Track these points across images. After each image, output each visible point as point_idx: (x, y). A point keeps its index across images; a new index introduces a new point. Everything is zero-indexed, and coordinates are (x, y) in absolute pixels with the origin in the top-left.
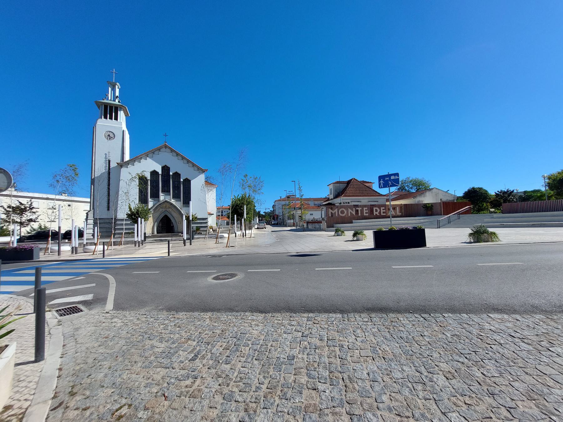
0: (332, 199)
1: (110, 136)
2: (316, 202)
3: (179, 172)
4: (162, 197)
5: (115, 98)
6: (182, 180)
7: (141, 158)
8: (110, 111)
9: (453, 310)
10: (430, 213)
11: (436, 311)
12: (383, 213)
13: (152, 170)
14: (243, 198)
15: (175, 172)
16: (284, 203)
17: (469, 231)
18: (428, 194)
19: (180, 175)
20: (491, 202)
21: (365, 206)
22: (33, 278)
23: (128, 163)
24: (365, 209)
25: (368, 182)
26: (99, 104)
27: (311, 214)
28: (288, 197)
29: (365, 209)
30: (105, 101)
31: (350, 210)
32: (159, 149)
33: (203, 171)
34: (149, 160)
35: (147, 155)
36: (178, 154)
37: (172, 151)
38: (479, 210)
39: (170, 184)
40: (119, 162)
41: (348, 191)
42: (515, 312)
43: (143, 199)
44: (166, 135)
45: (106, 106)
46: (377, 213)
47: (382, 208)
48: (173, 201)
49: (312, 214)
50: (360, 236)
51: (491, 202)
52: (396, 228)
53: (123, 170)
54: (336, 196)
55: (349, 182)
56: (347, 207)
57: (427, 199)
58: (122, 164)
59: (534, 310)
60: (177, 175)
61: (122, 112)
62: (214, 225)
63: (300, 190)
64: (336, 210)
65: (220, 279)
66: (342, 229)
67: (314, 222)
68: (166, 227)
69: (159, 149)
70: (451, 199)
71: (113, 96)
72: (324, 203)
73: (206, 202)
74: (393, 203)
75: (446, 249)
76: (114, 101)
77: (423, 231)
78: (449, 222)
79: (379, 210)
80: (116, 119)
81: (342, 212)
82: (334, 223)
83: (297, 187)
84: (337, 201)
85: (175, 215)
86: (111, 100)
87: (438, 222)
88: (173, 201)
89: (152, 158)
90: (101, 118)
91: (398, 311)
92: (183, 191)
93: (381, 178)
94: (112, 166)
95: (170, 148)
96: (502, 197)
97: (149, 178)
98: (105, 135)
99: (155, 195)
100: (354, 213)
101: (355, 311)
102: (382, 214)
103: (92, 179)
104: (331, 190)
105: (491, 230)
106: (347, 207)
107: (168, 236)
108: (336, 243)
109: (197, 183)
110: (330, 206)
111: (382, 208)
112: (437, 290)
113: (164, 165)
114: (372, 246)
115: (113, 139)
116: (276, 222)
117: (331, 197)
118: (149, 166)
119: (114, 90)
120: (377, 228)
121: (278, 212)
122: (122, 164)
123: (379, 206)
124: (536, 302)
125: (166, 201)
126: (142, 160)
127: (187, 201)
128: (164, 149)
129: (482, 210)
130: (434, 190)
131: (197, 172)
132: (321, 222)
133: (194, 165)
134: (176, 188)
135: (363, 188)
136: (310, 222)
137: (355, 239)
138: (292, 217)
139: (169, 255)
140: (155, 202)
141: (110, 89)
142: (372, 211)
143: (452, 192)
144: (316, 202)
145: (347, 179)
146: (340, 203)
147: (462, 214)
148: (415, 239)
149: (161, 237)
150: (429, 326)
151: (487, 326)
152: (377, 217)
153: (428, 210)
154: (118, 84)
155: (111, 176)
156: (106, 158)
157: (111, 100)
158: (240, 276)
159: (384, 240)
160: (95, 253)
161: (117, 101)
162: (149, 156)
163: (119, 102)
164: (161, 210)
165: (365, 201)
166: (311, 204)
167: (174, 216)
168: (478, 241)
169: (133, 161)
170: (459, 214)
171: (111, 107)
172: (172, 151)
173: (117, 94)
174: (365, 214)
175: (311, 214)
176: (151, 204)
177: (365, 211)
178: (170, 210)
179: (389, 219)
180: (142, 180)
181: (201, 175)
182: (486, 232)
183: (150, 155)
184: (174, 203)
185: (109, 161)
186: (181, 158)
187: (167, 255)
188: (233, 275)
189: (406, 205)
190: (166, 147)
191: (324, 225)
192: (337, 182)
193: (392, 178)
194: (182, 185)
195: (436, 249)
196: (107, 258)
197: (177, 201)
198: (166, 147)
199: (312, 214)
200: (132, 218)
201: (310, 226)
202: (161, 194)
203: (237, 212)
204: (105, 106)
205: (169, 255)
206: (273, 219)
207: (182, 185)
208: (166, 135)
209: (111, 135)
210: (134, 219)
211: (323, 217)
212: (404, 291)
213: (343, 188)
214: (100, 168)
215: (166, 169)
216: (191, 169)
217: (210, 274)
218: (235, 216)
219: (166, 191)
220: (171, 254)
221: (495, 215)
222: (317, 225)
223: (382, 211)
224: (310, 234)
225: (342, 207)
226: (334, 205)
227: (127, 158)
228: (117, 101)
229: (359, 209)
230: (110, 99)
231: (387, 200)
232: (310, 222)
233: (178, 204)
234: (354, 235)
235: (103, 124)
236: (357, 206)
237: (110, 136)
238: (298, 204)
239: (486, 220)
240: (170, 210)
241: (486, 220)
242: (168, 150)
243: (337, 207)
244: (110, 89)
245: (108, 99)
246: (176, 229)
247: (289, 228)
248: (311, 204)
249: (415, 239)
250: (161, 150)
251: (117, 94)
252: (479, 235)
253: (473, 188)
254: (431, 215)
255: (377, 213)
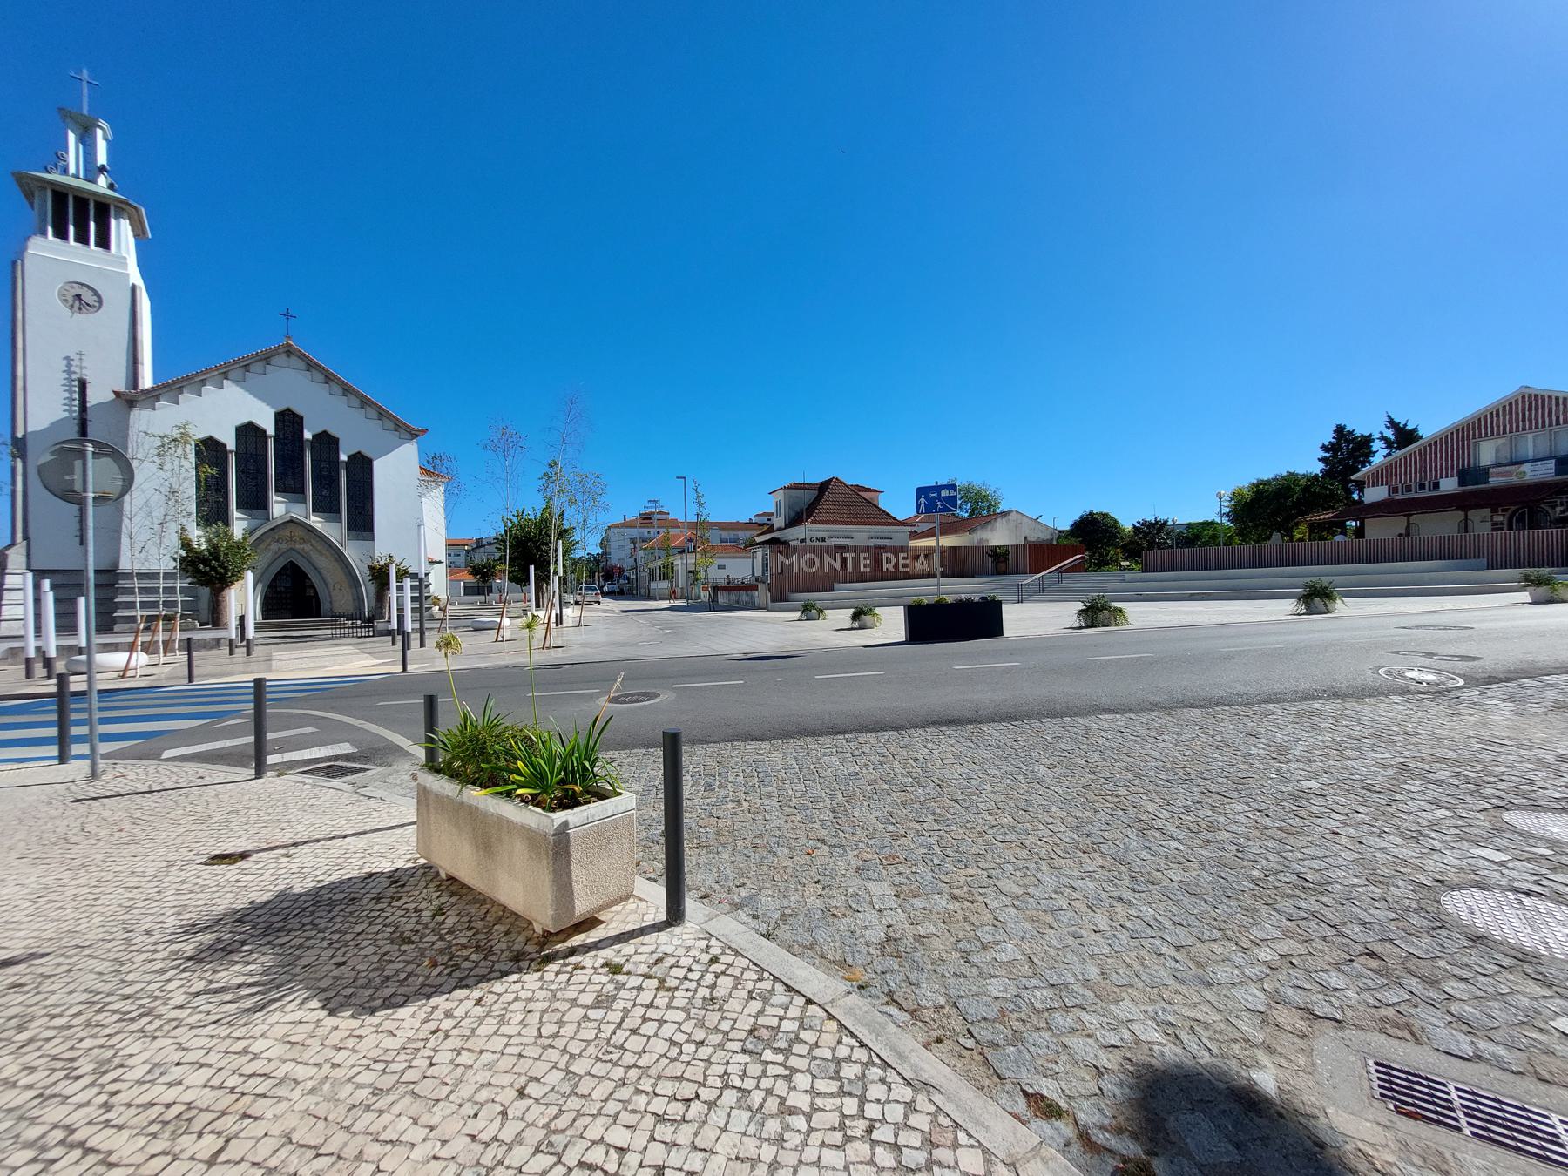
0: (779, 529)
1: (82, 299)
2: (725, 535)
3: (333, 432)
4: (279, 507)
5: (92, 171)
6: (343, 457)
7: (203, 383)
8: (79, 215)
9: (1052, 714)
10: (1003, 567)
11: (1030, 718)
12: (905, 566)
13: (243, 420)
14: (543, 524)
15: (320, 430)
16: (634, 532)
17: (1080, 606)
18: (1000, 523)
19: (336, 441)
20: (1124, 547)
21: (866, 549)
22: (53, 732)
23: (153, 396)
24: (862, 555)
25: (869, 490)
26: (29, 187)
27: (721, 567)
28: (646, 518)
29: (862, 555)
30: (55, 177)
31: (827, 559)
32: (266, 358)
33: (413, 434)
34: (231, 390)
35: (223, 373)
36: (329, 378)
37: (311, 365)
38: (1101, 564)
39: (305, 464)
40: (122, 388)
41: (823, 509)
42: (1130, 711)
43: (212, 511)
44: (288, 316)
45: (60, 195)
46: (890, 566)
47: (901, 555)
48: (315, 521)
49: (723, 567)
50: (867, 619)
51: (1124, 547)
52: (949, 599)
53: (141, 419)
54: (794, 521)
55: (823, 487)
56: (820, 552)
57: (998, 536)
58: (130, 398)
59: (1154, 706)
60: (326, 442)
61: (125, 224)
62: (443, 596)
63: (699, 500)
64: (795, 558)
65: (643, 694)
66: (819, 604)
67: (731, 587)
68: (295, 600)
69: (266, 358)
70: (1044, 536)
71: (84, 161)
72: (758, 539)
73: (417, 521)
74: (930, 542)
75: (1040, 639)
76: (94, 181)
77: (1000, 604)
78: (1041, 590)
79: (894, 560)
80: (104, 242)
81: (810, 563)
82: (789, 588)
83: (691, 495)
84: (796, 534)
85: (324, 562)
86: (76, 176)
87: (1020, 588)
88: (315, 521)
89: (241, 382)
90: (44, 233)
91: (978, 721)
92: (349, 490)
93: (921, 492)
94: (94, 398)
95: (302, 356)
96: (1146, 535)
97: (231, 445)
98: (60, 294)
99: (255, 501)
100: (838, 566)
101: (915, 726)
102: (862, 569)
103: (15, 440)
104: (778, 505)
105: (1114, 604)
106: (820, 552)
107: (308, 627)
108: (821, 635)
109: (395, 472)
110: (775, 547)
111: (901, 555)
112: (1031, 692)
113: (282, 408)
114: (901, 636)
115: (90, 309)
116: (616, 588)
117: (778, 522)
118: (226, 410)
119: (87, 140)
120: (910, 601)
121: (615, 560)
122: (130, 398)
123: (896, 550)
124: (1151, 698)
125: (292, 521)
126: (208, 389)
127: (362, 523)
128: (281, 359)
129: (1107, 564)
130: (1013, 516)
131: (392, 437)
132: (756, 588)
133: (382, 414)
134: (327, 482)
135: (858, 504)
136: (724, 588)
137: (856, 625)
138: (667, 573)
139: (405, 669)
140: (257, 522)
141: (72, 137)
142: (877, 562)
143: (1047, 521)
144: (725, 535)
145: (816, 479)
146: (803, 541)
147: (1066, 571)
148: (981, 621)
149: (280, 628)
150: (1024, 732)
151: (1094, 726)
152: (890, 577)
153: (999, 561)
154: (102, 123)
155: (92, 433)
156: (69, 372)
157: (76, 176)
158: (664, 697)
159: (929, 624)
160: (129, 673)
161: (102, 181)
162: (231, 375)
163: (111, 186)
164: (275, 547)
165: (861, 535)
166: (714, 537)
167: (322, 571)
168: (1092, 624)
169: (168, 389)
170: (1061, 571)
171: (82, 201)
172: (311, 365)
173: (102, 158)
174: (862, 569)
175: (721, 567)
176: (239, 525)
177: (862, 562)
178: (307, 547)
179: (934, 581)
180: (210, 450)
181: (407, 446)
182: (1105, 607)
183: (237, 374)
184: (318, 526)
185: (83, 385)
186: (340, 391)
187: (400, 668)
188: (651, 696)
189: (952, 549)
190: (289, 351)
191: (763, 594)
192: (796, 486)
193: (944, 493)
194: (343, 473)
195: (1021, 640)
196: (198, 683)
197: (327, 520)
198: (289, 351)
199: (723, 567)
200: (199, 571)
201: (722, 599)
202: (274, 497)
203: (519, 558)
204: (75, 198)
205: (405, 669)
206: (610, 579)
207: (343, 473)
208: (288, 316)
209: (88, 297)
210: (205, 573)
211: (758, 573)
212: (985, 697)
213: (812, 501)
214: (45, 408)
215: (289, 421)
216: (375, 426)
217: (598, 695)
218: (532, 568)
219: (291, 486)
220: (410, 668)
221: (1128, 575)
222: (743, 596)
223: (901, 562)
224: (751, 620)
225: (812, 550)
226: (786, 543)
227: (147, 381)
228: (102, 181)
229: (850, 556)
230: (72, 170)
231: (915, 535)
232: (724, 588)
233: (333, 530)
234: (855, 617)
235: (51, 257)
236: (842, 548)
237: (82, 299)
238: (676, 537)
239: (1110, 585)
240: (307, 547)
241: (1110, 585)
242: (294, 360)
243: (795, 549)
244: (72, 137)
245: (65, 171)
246: (325, 606)
247: (666, 604)
248: (714, 537)
249: (981, 621)
250: (274, 360)
251: (102, 158)
252: (1095, 614)
253: (1091, 514)
254: (1005, 573)
255: (890, 566)
